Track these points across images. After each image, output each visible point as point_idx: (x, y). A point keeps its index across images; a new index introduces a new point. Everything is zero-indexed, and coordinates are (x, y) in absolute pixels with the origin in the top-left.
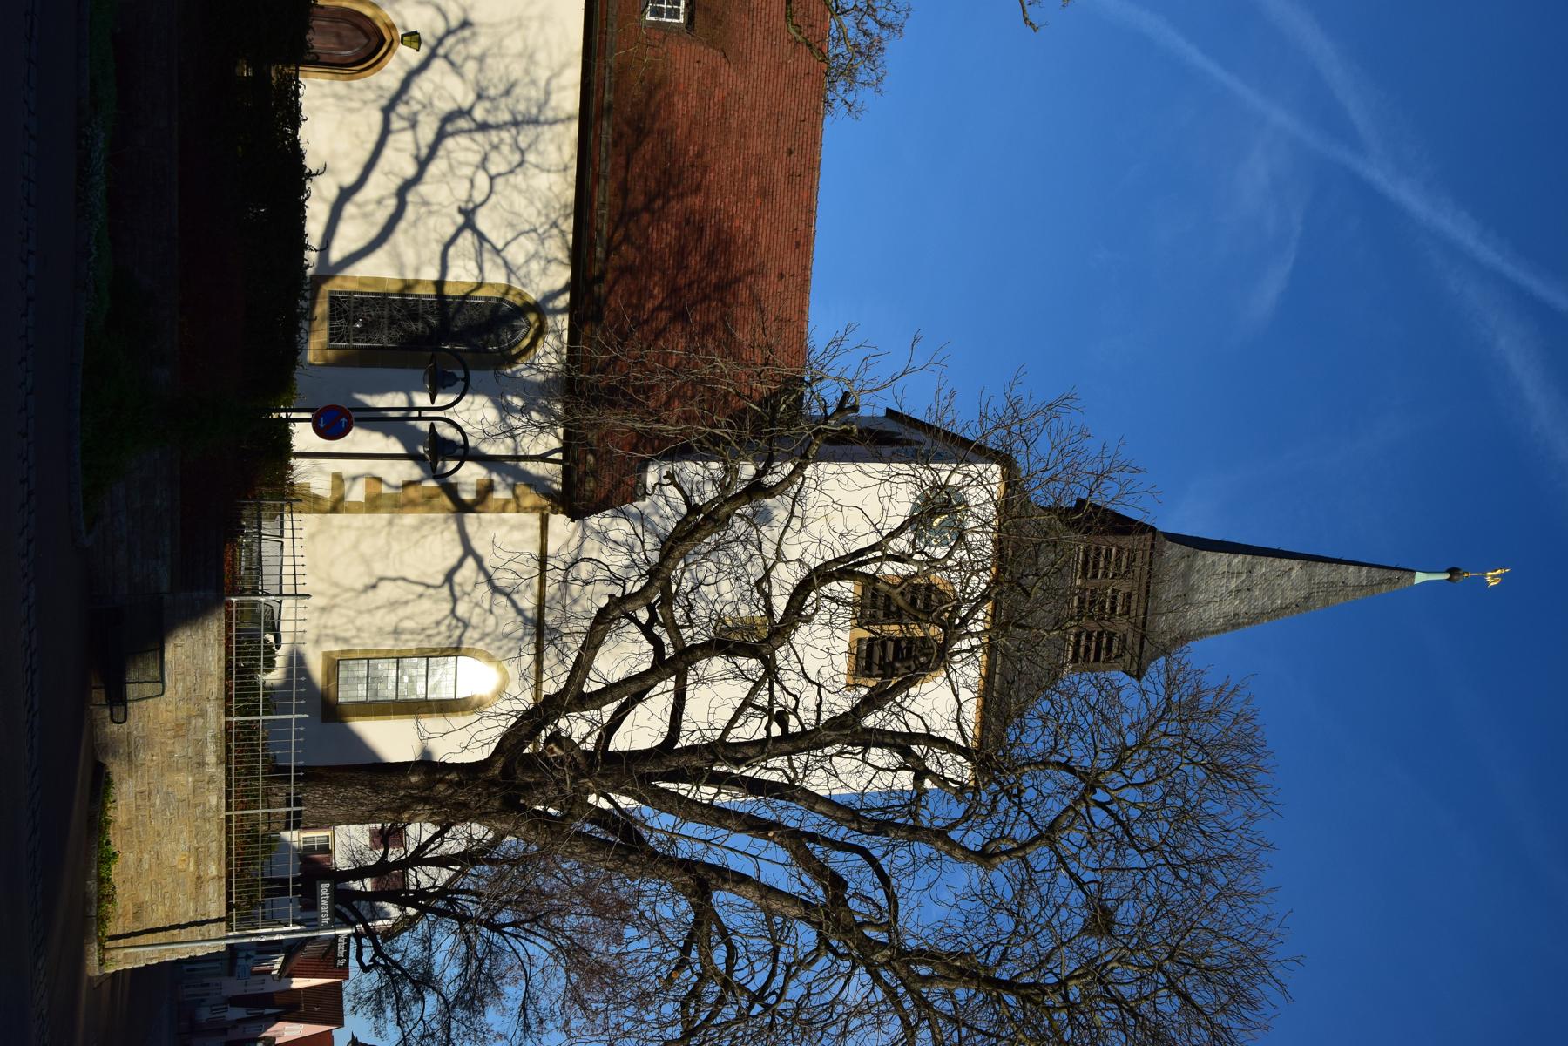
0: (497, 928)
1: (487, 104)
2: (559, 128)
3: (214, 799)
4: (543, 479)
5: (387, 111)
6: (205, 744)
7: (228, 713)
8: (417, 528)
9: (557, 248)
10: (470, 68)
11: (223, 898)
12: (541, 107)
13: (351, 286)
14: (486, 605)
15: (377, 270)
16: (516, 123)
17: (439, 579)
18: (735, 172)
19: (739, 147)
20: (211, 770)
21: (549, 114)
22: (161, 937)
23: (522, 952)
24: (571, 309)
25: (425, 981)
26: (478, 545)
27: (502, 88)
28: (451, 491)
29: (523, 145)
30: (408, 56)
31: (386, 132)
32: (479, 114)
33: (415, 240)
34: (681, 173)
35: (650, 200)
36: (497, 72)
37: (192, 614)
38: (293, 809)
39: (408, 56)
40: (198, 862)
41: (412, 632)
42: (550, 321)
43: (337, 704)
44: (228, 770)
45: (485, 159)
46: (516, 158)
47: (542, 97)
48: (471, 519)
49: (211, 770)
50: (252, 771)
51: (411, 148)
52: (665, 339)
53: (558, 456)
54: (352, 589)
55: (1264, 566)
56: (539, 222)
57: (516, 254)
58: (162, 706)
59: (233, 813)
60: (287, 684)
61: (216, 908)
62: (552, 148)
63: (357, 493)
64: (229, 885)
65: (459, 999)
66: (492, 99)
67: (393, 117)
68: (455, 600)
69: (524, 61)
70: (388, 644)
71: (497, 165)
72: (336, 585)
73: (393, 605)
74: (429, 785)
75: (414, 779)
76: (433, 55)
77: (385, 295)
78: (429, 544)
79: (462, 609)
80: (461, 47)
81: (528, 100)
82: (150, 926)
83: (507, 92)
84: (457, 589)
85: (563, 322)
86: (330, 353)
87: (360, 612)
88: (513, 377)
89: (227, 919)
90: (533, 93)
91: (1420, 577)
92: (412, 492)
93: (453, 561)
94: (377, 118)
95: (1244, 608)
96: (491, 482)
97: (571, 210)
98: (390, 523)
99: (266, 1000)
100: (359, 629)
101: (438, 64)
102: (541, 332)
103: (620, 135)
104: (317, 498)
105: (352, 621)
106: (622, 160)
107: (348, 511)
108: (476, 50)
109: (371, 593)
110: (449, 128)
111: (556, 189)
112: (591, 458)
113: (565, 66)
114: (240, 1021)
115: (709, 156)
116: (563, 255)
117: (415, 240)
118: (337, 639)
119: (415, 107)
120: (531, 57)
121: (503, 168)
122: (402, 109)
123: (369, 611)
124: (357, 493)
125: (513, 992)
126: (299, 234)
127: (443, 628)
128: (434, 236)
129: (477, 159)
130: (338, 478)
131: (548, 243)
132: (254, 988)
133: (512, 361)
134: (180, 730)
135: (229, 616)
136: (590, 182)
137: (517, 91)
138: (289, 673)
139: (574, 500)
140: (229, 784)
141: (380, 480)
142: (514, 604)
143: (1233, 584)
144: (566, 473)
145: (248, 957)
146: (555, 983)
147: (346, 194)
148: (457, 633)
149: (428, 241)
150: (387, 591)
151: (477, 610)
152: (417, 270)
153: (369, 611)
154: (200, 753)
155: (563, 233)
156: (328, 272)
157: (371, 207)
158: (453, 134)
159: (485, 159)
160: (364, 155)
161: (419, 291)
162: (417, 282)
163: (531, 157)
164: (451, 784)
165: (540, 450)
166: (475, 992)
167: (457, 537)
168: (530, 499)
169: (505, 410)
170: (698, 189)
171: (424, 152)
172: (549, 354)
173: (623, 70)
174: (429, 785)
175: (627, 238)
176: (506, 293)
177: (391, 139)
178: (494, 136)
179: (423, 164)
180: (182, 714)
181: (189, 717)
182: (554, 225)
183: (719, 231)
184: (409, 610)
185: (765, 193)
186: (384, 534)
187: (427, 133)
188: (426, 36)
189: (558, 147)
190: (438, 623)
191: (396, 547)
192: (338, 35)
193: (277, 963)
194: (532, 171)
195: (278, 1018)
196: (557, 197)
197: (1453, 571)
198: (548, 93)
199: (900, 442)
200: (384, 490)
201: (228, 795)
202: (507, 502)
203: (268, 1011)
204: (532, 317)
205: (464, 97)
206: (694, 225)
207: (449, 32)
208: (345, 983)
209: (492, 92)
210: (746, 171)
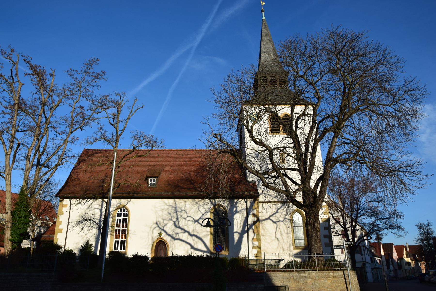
0: (358, 209)
1: (173, 218)
2: (177, 203)
3: (314, 274)
4: (251, 203)
5: (175, 239)
6: (300, 276)
7: (293, 271)
8: (264, 230)
9: (201, 202)
10: (165, 222)
11: (338, 271)
12: (173, 207)
13: (212, 246)
14: (281, 214)
15: (208, 240)
16: (176, 212)
17: (275, 224)
18: (186, 166)
19: (182, 166)
20: (306, 275)
21: (174, 205)
22: (348, 286)
23: (363, 203)
24: (214, 198)
25: (373, 224)
26: (267, 216)
27: (169, 215)
28: (254, 223)
29: (181, 210)
30: (164, 235)
31: (179, 239)
32: (175, 220)
33: (201, 233)
34: (186, 177)
35: (192, 183)
36: (166, 217)
37: (269, 280)
38: (316, 255)
39: (163, 235)
40: (329, 277)
41: (287, 230)
42: (217, 203)
43: (305, 246)
44: (307, 271)
45: (184, 218)
46: (183, 212)
47: (170, 207)
48: (260, 218)
49: (306, 275)
50: (307, 265)
51: (182, 234)
52: (220, 179)
53: (246, 200)
54: (279, 244)
55: (263, 50)
56: (196, 207)
57: (203, 211)
58: (291, 286)
59: (317, 269)
60: (300, 257)
61: (341, 273)
62: (181, 204)
63: (256, 243)
64: (335, 270)
65: (376, 217)
66: (172, 217)
67: (176, 238)
68: (280, 221)
69: (164, 211)
70: (291, 235)
71: (185, 215)
72: (278, 247)
73: (281, 234)
74: (310, 224)
75: (309, 228)
76: (163, 230)
77: (213, 238)
78: (267, 228)
79: (282, 219)
80: (161, 224)
81: (171, 210)
82: (346, 288)
83: (170, 214)
84: (277, 221)
85: (217, 200)
86: (226, 250)
87: (284, 242)
88: (229, 210)
89: (343, 270)
90: (170, 209)
91: (264, 18)
92: (255, 231)
93: (271, 222)
94: (176, 241)
95: (272, 53)
96: (252, 214)
97: (193, 200)
98: (263, 236)
99: (387, 261)
100: (288, 242)
101: (165, 229)
102: (220, 205)
103: (178, 190)
104: (258, 252)
105: (286, 243)
106: (183, 190)
107: (260, 245)
108: (162, 221)
109: (279, 240)
110: (178, 226)
111: (189, 203)
112: (246, 193)
113: (164, 203)
114: (393, 266)
115: (183, 172)
116: (203, 201)
117: (201, 233)
118: (290, 247)
119: (174, 233)
120: (163, 209)
121: (185, 214)
122: (174, 236)
123: (283, 240)
124: (256, 243)
125: (375, 204)
126: (198, 257)
127: (286, 223)
128: (200, 228)
129: (184, 220)
130: (253, 247)
131: (201, 204)
132: (385, 264)
133: (226, 211)
134: (297, 282)
135: (269, 271)
136: (187, 196)
137: (170, 212)
138: (298, 257)
139: (255, 196)
140: (311, 270)
141: (253, 238)
142: (280, 208)
143: (268, 56)
144: (249, 198)
145: (376, 265)
146: (371, 195)
147: (192, 247)
148: (287, 220)
149: (201, 230)
150: (278, 236)
151: (282, 216)
152: (207, 232)
153: (283, 240)
154: (302, 277)
155: (198, 201)
156: (209, 251)
157: (195, 242)
158: (179, 225)
159: (184, 218)
160: (184, 244)
161: (212, 231)
162: (210, 232)
163: (183, 209)
164: (310, 219)
165: (245, 204)
166: (374, 213)
167: (266, 221)
168: (255, 205)
169: (236, 212)
170: (189, 174)
171: (183, 231)
172: (226, 204)
173: (165, 191)
174: (310, 224)
175: (199, 188)
176: (212, 213)
177: (181, 238)
178: (179, 216)
179: (185, 231)
180: (293, 281)
181: (294, 280)
182: (197, 203)
183: (198, 169)
184: (282, 231)
185: (191, 160)
186: (266, 237)
187: (179, 231)
188: (159, 232)
189: (180, 202)
190: (285, 224)
191: (269, 234)
192: (160, 250)
193: (377, 259)
194: (186, 208)
195: (392, 258)
196: (191, 203)
197: (262, 12)
198: (170, 206)
199: (241, 128)
200: (255, 237)
201: (313, 270)
202: (256, 210)
203: (390, 260)
204: (217, 207)
205: (171, 223)
206: (197, 174)
207: (158, 227)
208: (395, 244)
209: (170, 217)
210: (186, 164)
